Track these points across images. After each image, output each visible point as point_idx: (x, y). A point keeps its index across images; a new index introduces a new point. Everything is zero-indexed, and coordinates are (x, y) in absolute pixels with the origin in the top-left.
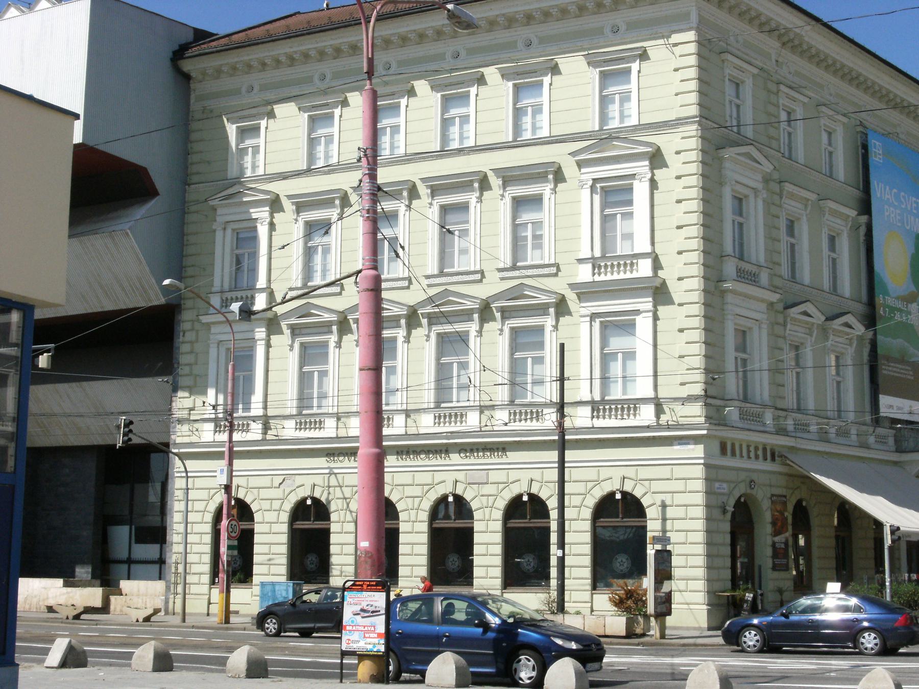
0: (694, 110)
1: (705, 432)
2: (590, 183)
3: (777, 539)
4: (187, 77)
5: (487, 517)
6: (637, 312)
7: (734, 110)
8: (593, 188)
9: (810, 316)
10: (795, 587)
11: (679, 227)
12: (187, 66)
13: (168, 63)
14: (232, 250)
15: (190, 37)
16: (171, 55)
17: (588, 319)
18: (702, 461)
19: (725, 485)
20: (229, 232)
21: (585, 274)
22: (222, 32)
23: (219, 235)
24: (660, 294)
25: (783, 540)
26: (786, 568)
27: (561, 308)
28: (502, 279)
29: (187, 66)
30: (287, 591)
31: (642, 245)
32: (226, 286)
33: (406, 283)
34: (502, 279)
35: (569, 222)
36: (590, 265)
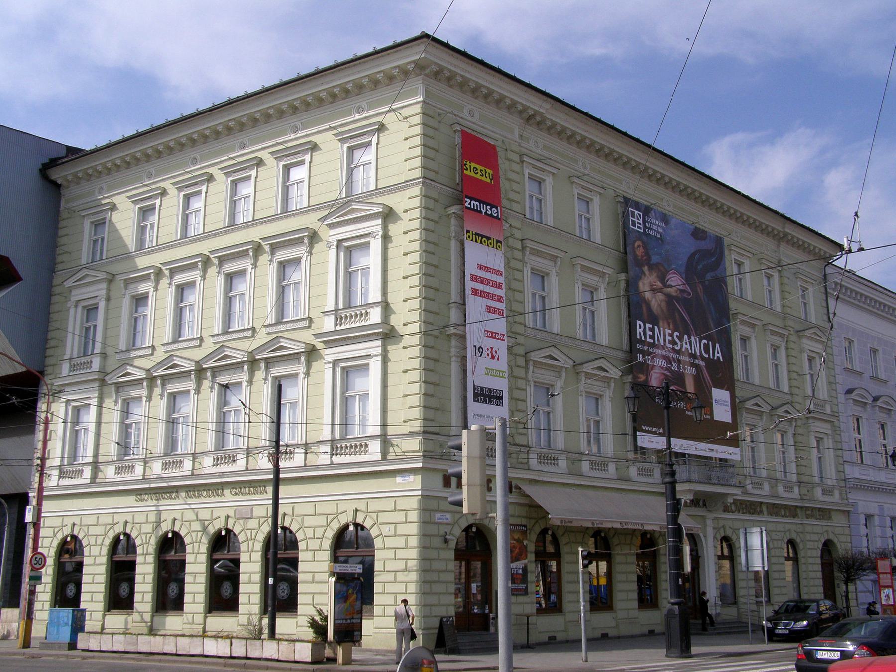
0: (418, 173)
1: (420, 465)
2: (335, 244)
3: (513, 565)
4: (58, 186)
5: (196, 551)
6: (369, 356)
7: (535, 205)
8: (337, 247)
9: (556, 360)
10: (639, 606)
11: (405, 278)
12: (57, 174)
13: (36, 172)
14: (82, 323)
15: (63, 153)
16: (40, 166)
17: (331, 365)
18: (419, 493)
19: (448, 516)
20: (80, 309)
21: (328, 324)
22: (88, 147)
23: (72, 311)
24: (389, 336)
25: (522, 566)
26: (526, 592)
27: (311, 353)
28: (268, 334)
29: (57, 174)
30: (68, 616)
31: (375, 295)
32: (75, 355)
33: (197, 343)
34: (268, 334)
35: (318, 282)
36: (333, 316)
